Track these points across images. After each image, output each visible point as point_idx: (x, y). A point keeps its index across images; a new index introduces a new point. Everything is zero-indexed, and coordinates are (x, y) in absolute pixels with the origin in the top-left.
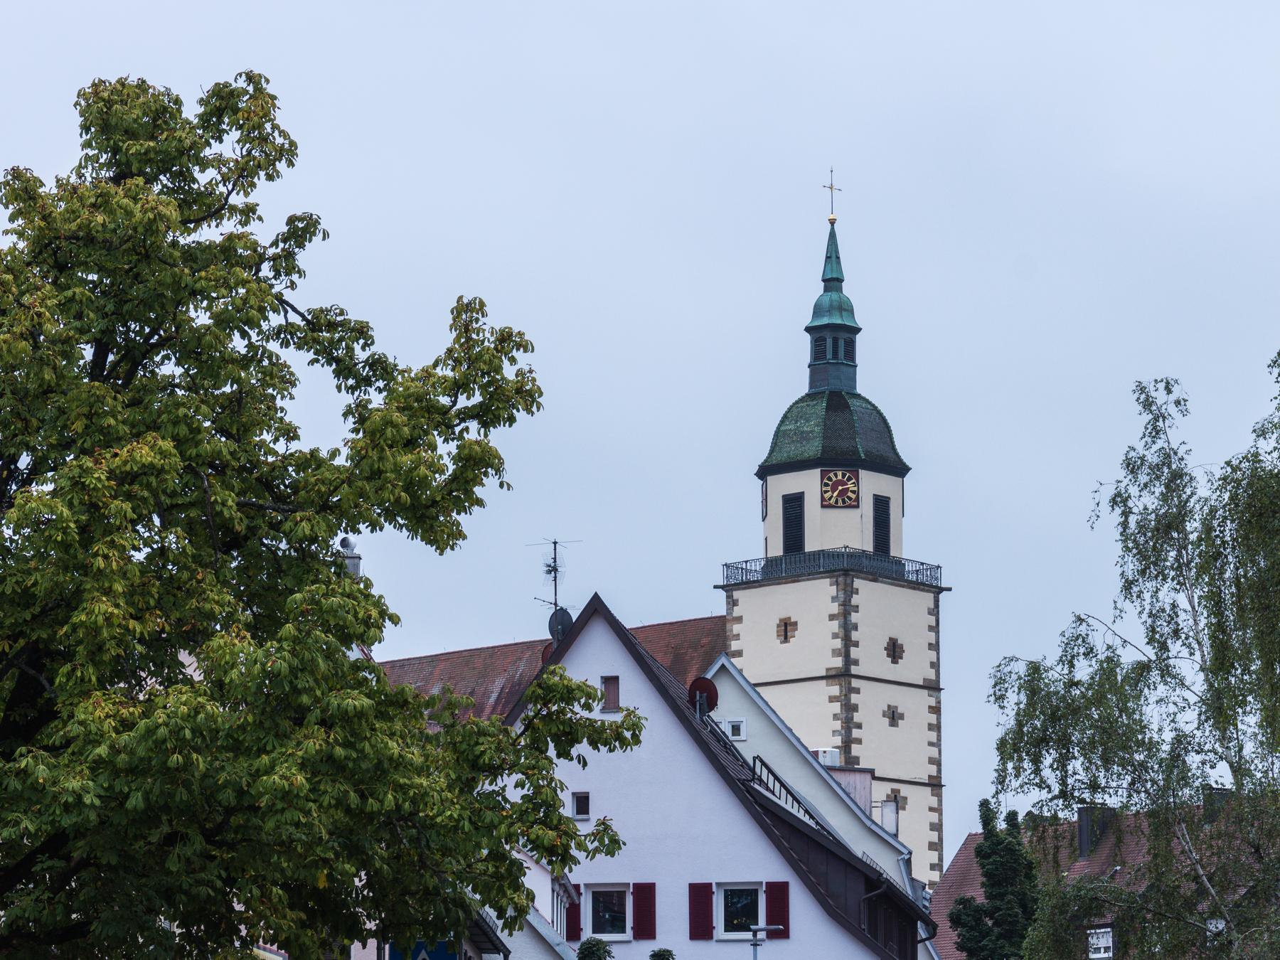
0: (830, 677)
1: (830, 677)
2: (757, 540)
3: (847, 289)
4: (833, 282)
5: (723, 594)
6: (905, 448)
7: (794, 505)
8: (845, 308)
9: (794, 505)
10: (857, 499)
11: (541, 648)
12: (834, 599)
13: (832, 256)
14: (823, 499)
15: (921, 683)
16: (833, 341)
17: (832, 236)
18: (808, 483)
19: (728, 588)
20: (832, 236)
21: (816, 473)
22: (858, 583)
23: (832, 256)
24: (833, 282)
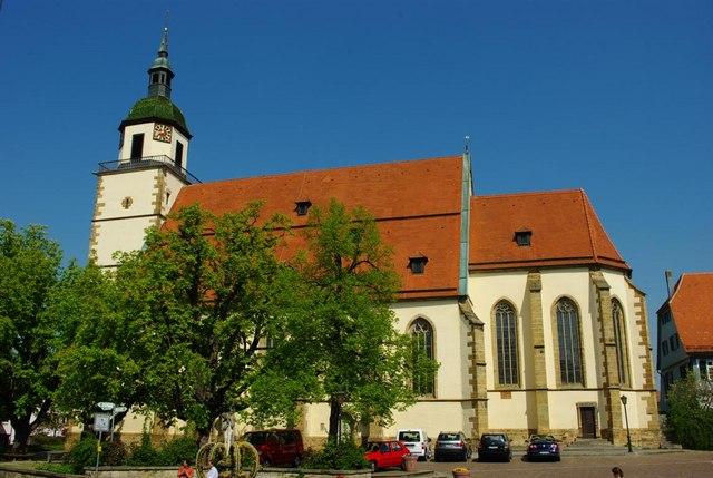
12: (156, 187)
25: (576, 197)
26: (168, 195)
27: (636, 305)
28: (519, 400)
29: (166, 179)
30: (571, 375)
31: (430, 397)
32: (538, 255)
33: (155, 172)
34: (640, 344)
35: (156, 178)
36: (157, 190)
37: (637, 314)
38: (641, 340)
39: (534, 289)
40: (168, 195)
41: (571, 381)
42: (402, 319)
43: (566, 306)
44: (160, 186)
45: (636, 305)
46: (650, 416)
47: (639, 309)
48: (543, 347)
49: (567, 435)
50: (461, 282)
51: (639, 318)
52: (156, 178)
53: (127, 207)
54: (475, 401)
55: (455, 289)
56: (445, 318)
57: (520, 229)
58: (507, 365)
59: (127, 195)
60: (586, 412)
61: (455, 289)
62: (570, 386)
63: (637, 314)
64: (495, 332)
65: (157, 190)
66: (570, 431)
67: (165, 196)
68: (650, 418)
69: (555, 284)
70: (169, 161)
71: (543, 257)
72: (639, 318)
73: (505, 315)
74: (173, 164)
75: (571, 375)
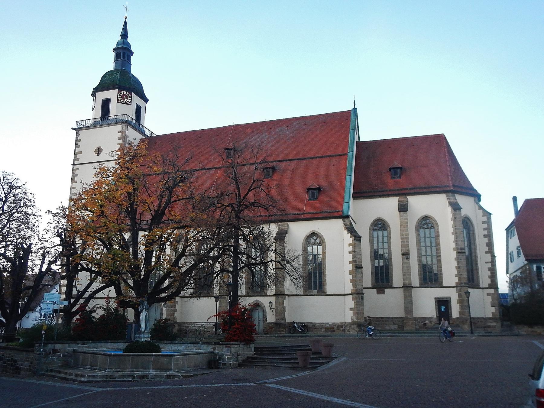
0: (491, 262)
1: (491, 262)
3: (129, 40)
5: (75, 132)
7: (106, 103)
9: (106, 103)
12: (119, 139)
15: (487, 286)
18: (112, 94)
21: (116, 91)
22: (129, 128)
25: (439, 141)
27: (484, 222)
33: (119, 127)
34: (487, 252)
35: (119, 132)
36: (120, 141)
37: (484, 229)
38: (487, 249)
39: (403, 208)
42: (299, 231)
43: (426, 223)
45: (484, 222)
46: (494, 308)
49: (427, 322)
50: (345, 206)
52: (119, 132)
53: (98, 154)
54: (358, 294)
56: (332, 230)
57: (397, 164)
63: (484, 229)
66: (430, 319)
68: (493, 309)
69: (422, 205)
70: (131, 120)
72: (486, 232)
74: (134, 122)
75: (315, 283)
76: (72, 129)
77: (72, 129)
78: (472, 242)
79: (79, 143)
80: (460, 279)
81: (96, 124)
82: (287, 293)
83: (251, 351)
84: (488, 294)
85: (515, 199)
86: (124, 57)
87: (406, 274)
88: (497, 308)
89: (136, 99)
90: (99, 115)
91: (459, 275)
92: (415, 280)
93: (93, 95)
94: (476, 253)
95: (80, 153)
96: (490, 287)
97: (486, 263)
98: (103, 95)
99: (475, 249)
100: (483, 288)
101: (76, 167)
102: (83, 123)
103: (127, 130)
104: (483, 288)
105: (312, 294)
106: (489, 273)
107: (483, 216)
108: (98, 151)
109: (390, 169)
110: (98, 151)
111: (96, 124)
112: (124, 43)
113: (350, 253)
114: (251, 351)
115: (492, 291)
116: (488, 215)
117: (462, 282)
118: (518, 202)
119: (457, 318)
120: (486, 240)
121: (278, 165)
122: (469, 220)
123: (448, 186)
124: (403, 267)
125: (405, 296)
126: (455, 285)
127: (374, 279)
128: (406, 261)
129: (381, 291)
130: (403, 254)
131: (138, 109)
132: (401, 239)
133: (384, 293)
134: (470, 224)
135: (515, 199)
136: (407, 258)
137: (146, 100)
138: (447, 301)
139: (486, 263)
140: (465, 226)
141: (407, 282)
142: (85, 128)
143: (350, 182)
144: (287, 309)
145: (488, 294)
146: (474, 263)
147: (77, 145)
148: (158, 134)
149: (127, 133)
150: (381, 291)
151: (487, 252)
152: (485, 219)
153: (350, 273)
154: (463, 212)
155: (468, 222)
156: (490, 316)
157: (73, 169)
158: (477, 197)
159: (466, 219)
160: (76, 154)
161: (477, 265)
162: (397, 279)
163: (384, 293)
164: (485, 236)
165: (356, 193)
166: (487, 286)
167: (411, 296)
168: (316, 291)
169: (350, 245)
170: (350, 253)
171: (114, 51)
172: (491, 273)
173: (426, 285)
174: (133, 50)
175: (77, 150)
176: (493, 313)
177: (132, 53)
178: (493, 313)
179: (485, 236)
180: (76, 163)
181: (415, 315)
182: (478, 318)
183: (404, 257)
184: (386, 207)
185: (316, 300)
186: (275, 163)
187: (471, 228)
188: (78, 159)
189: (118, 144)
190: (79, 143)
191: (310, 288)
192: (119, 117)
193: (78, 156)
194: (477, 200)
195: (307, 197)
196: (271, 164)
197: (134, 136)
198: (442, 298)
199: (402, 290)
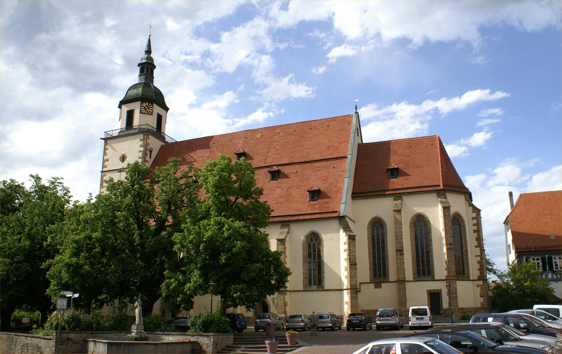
0: (480, 256)
1: (480, 256)
2: (117, 124)
3: (152, 55)
4: (149, 52)
5: (103, 141)
6: (168, 101)
7: (130, 114)
8: (152, 59)
9: (130, 114)
10: (152, 112)
11: (350, 241)
12: (141, 146)
13: (149, 45)
14: (141, 111)
15: (477, 278)
16: (147, 68)
17: (149, 40)
18: (136, 107)
19: (106, 140)
20: (149, 40)
21: (139, 103)
22: (150, 136)
23: (149, 45)
24: (149, 52)
26: (151, 151)
27: (473, 218)
28: (388, 290)
29: (149, 141)
30: (424, 270)
31: (429, 278)
32: (265, 163)
34: (476, 247)
36: (142, 149)
38: (476, 243)
40: (151, 151)
41: (424, 274)
44: (145, 146)
45: (473, 218)
46: (482, 298)
47: (475, 221)
48: (402, 250)
51: (475, 228)
53: (123, 161)
54: (355, 290)
55: (337, 212)
58: (379, 265)
59: (123, 153)
60: (434, 297)
61: (337, 212)
62: (423, 278)
64: (371, 242)
65: (142, 149)
67: (148, 152)
68: (482, 300)
70: (152, 128)
71: (405, 186)
72: (475, 228)
73: (377, 229)
75: (424, 270)
76: (101, 139)
77: (101, 139)
78: (463, 237)
79: (107, 151)
80: (448, 272)
81: (121, 136)
82: (407, 280)
83: (230, 341)
84: (478, 286)
85: (511, 194)
86: (147, 71)
87: (401, 268)
88: (485, 298)
89: (157, 109)
90: (124, 126)
91: (448, 269)
92: (409, 274)
93: (120, 107)
94: (466, 247)
95: (107, 160)
96: (479, 279)
97: (476, 256)
98: (125, 108)
99: (466, 244)
100: (473, 280)
101: (104, 174)
102: (110, 133)
103: (149, 138)
104: (473, 280)
105: (311, 289)
106: (478, 266)
107: (473, 212)
108: (123, 158)
109: (388, 170)
110: (123, 158)
111: (121, 136)
112: (147, 58)
113: (345, 251)
114: (230, 341)
115: (481, 282)
116: (477, 211)
117: (451, 275)
118: (513, 197)
119: (447, 309)
120: (476, 235)
121: (284, 170)
122: (460, 216)
123: (439, 186)
124: (397, 263)
125: (399, 290)
126: (445, 278)
127: (372, 274)
128: (400, 256)
129: (378, 286)
130: (396, 251)
131: (160, 119)
132: (396, 236)
133: (381, 287)
134: (461, 220)
135: (511, 194)
136: (401, 255)
137: (167, 109)
138: (439, 293)
139: (476, 256)
140: (455, 223)
141: (401, 277)
142: (113, 138)
143: (347, 184)
144: (288, 304)
145: (478, 286)
146: (465, 257)
147: (105, 154)
148: (178, 140)
149: (149, 141)
150: (378, 286)
151: (476, 247)
152: (474, 215)
153: (346, 270)
154: (452, 211)
155: (459, 218)
156: (480, 306)
157: (102, 176)
158: (468, 195)
159: (457, 216)
160: (104, 161)
161: (467, 258)
162: (392, 274)
163: (381, 287)
164: (475, 231)
165: (355, 193)
166: (477, 278)
167: (405, 289)
168: (315, 286)
169: (345, 244)
170: (345, 251)
171: (138, 66)
172: (480, 266)
173: (419, 279)
174: (155, 64)
175: (106, 157)
176: (481, 303)
177: (155, 67)
178: (481, 303)
179: (475, 231)
180: (104, 170)
181: (460, 306)
182: (468, 308)
183: (398, 253)
184: (382, 207)
185: (316, 296)
186: (279, 168)
187: (462, 224)
188: (106, 167)
189: (140, 152)
190: (107, 151)
191: (310, 284)
192: (141, 127)
193: (106, 163)
194: (468, 197)
195: (308, 199)
196: (276, 168)
197: (155, 144)
198: (434, 290)
199: (396, 284)
